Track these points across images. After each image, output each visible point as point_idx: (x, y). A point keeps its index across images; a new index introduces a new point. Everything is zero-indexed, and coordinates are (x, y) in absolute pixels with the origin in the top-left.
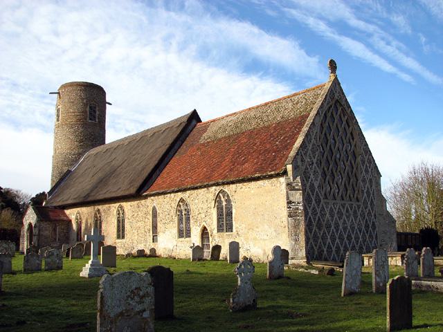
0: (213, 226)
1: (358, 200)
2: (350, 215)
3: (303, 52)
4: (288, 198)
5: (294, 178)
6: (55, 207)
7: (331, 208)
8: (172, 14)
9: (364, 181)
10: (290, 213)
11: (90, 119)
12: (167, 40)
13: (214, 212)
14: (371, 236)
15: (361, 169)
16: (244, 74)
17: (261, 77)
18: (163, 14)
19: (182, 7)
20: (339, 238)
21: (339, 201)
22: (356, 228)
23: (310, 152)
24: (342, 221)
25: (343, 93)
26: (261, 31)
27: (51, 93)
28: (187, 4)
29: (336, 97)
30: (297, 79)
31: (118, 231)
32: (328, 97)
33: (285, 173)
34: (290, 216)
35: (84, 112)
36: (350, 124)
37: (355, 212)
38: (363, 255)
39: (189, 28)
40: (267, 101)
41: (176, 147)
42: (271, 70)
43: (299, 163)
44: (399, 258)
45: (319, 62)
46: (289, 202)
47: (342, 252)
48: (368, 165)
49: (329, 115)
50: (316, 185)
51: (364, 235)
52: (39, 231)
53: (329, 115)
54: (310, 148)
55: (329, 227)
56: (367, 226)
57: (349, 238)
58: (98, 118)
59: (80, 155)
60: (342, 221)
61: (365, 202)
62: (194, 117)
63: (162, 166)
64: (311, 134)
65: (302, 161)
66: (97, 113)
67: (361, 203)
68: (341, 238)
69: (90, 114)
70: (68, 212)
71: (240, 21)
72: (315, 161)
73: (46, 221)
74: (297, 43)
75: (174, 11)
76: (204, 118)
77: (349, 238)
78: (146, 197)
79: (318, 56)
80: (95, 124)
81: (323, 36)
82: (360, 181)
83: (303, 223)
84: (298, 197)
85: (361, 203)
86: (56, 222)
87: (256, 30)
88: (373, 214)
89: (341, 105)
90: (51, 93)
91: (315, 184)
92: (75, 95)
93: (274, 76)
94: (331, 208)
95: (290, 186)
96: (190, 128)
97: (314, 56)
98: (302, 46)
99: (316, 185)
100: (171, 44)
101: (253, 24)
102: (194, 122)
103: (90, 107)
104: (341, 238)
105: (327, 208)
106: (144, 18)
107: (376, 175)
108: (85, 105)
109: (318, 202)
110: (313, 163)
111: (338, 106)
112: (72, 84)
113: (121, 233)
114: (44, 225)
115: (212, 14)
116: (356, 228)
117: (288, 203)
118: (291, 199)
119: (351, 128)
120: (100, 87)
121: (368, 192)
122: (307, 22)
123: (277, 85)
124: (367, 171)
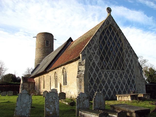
0: (62, 84)
1: (123, 69)
2: (118, 76)
3: (146, 16)
4: (78, 69)
5: (83, 60)
6: (31, 78)
7: (106, 73)
8: (94, 6)
9: (127, 60)
10: (78, 76)
11: (46, 45)
12: (93, 16)
13: (62, 76)
14: (131, 86)
15: (125, 55)
16: (124, 27)
17: (131, 27)
18: (90, 7)
19: (96, 3)
20: (110, 87)
21: (111, 70)
22: (122, 82)
23: (93, 48)
24: (112, 79)
25: (114, 21)
26: (128, 9)
27: (33, 37)
28: (98, 2)
29: (110, 23)
30: (145, 27)
31: (44, 87)
32: (105, 23)
33: (79, 58)
34: (77, 77)
35: (44, 43)
36: (119, 35)
37: (121, 75)
38: (116, 95)
39: (101, 11)
40: (89, 30)
41: (62, 52)
42: (134, 24)
43: (86, 53)
44: (129, 97)
45: (153, 19)
46: (79, 71)
47: (112, 94)
48: (130, 53)
49: (106, 32)
50: (96, 63)
51: (126, 86)
52: (23, 86)
53: (106, 32)
54: (93, 47)
55: (104, 82)
56: (129, 82)
57: (117, 87)
58: (50, 45)
59: (43, 58)
60: (112, 79)
61: (128, 71)
62: (70, 40)
63: (56, 60)
64: (94, 40)
65: (88, 52)
66: (49, 43)
67: (125, 71)
68: (112, 88)
69: (47, 43)
70: (35, 79)
71: (119, 6)
72: (96, 52)
73: (26, 83)
74: (143, 12)
75: (94, 5)
76: (74, 40)
77: (117, 87)
78: (48, 72)
79: (152, 17)
80: (48, 47)
81: (153, 8)
82: (125, 61)
83: (83, 80)
84: (83, 68)
85: (125, 71)
86: (29, 83)
87: (126, 9)
88: (133, 76)
89: (113, 27)
90: (33, 37)
91: (96, 63)
92: (41, 36)
93: (135, 26)
94: (106, 73)
95: (80, 64)
96: (68, 44)
97: (151, 17)
98: (145, 13)
99: (96, 63)
100: (95, 18)
101: (124, 6)
102: (70, 42)
103: (47, 41)
104: (112, 88)
105: (103, 73)
106: (83, 9)
107: (135, 58)
108: (45, 41)
109: (97, 70)
110: (95, 53)
111: (112, 27)
112: (40, 34)
113: (44, 88)
114: (25, 84)
115: (108, 5)
116: (122, 82)
117: (78, 71)
118: (80, 69)
119: (119, 37)
120: (46, 33)
121: (130, 65)
122: (146, 3)
123: (138, 30)
124: (129, 56)
